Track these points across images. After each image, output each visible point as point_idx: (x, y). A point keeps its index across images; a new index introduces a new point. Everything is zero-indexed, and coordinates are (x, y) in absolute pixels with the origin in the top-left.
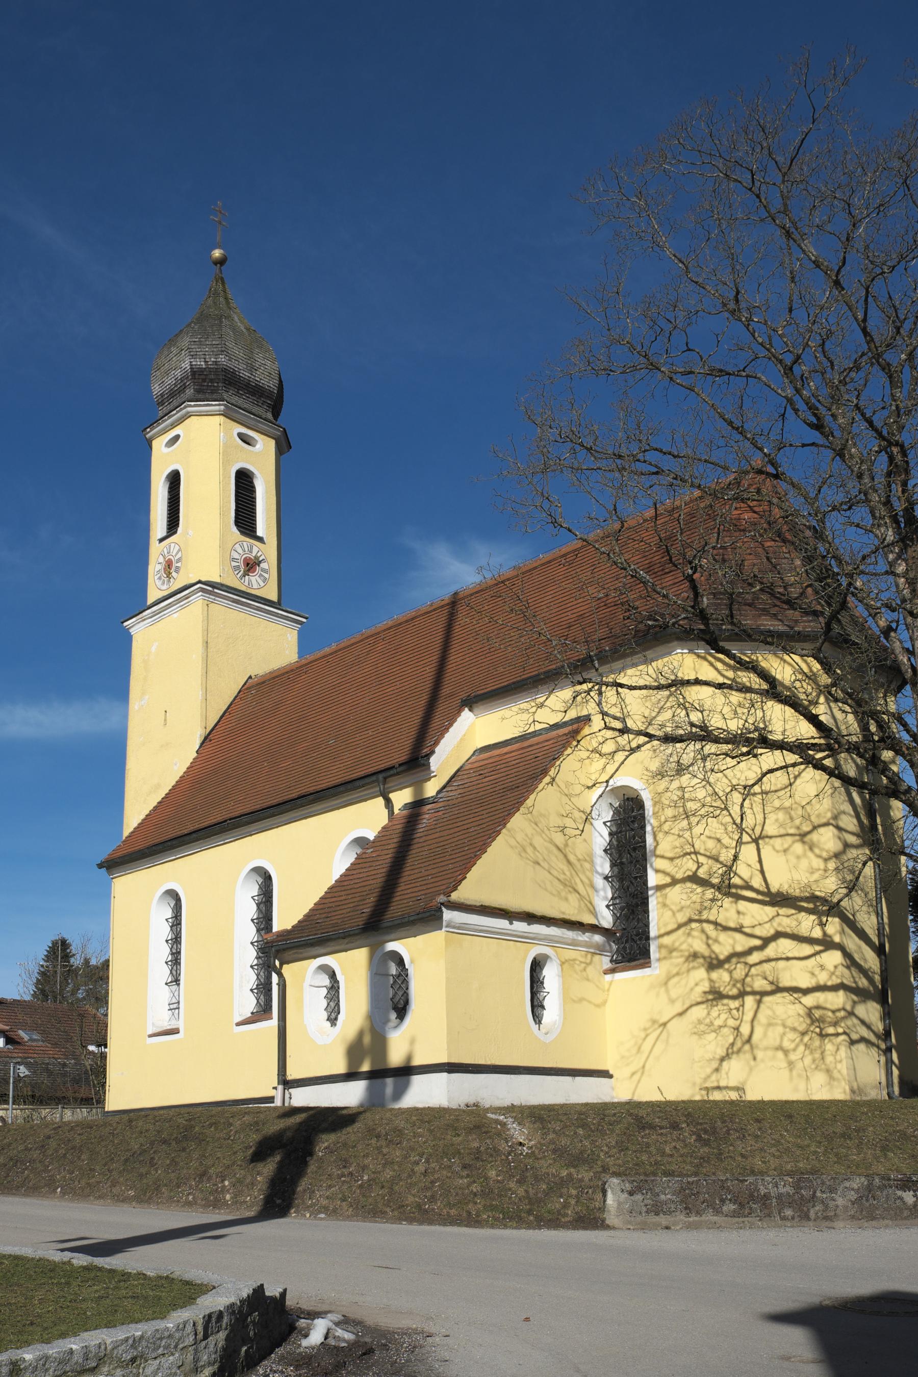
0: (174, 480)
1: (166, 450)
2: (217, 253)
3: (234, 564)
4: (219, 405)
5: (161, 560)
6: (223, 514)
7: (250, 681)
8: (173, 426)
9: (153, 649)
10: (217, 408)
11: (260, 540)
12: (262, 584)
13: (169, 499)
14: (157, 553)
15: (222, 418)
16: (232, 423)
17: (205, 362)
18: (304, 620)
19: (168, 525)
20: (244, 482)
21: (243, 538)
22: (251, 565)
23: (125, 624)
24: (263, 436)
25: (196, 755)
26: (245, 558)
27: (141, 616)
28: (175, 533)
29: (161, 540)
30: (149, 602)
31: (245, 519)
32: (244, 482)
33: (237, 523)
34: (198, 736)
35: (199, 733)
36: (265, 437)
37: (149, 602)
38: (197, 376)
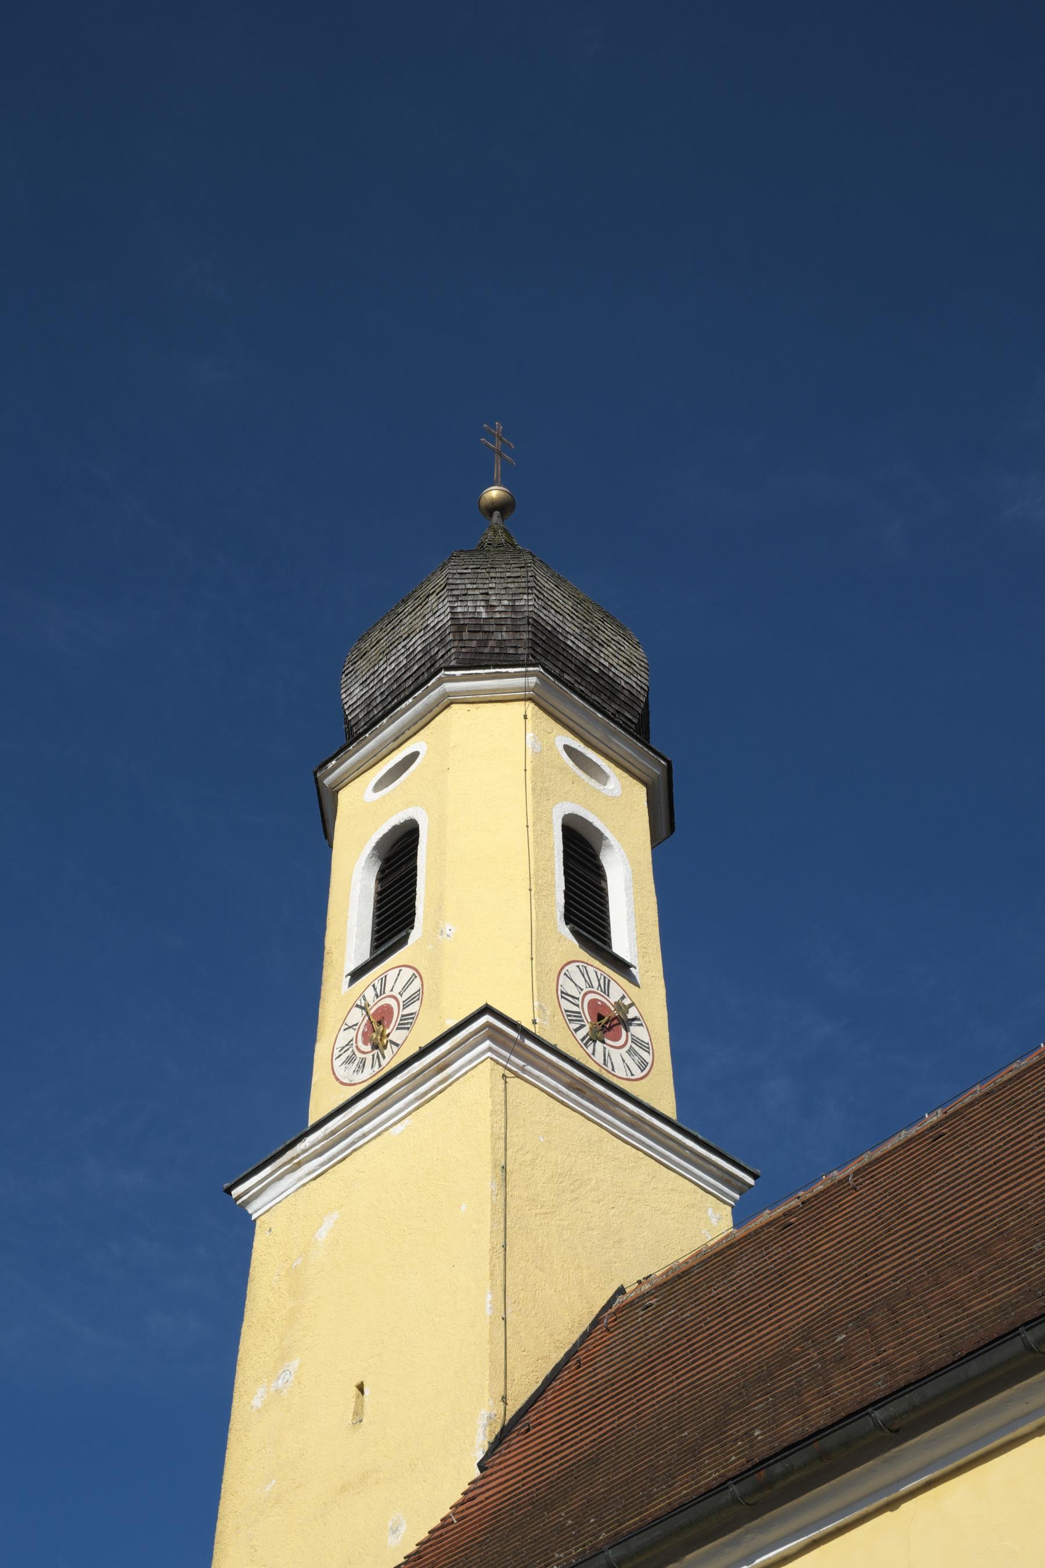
0: (399, 854)
2: (494, 493)
4: (525, 675)
6: (536, 890)
7: (620, 1299)
8: (400, 739)
9: (323, 1234)
10: (520, 681)
12: (638, 1074)
13: (379, 893)
15: (530, 707)
16: (552, 723)
18: (750, 1181)
20: (581, 849)
21: (584, 956)
22: (609, 1023)
23: (235, 1193)
24: (618, 771)
25: (476, 1473)
27: (290, 1154)
31: (586, 909)
32: (581, 849)
33: (569, 917)
34: (482, 1421)
35: (485, 1412)
36: (626, 775)
37: (312, 1121)
38: (466, 635)
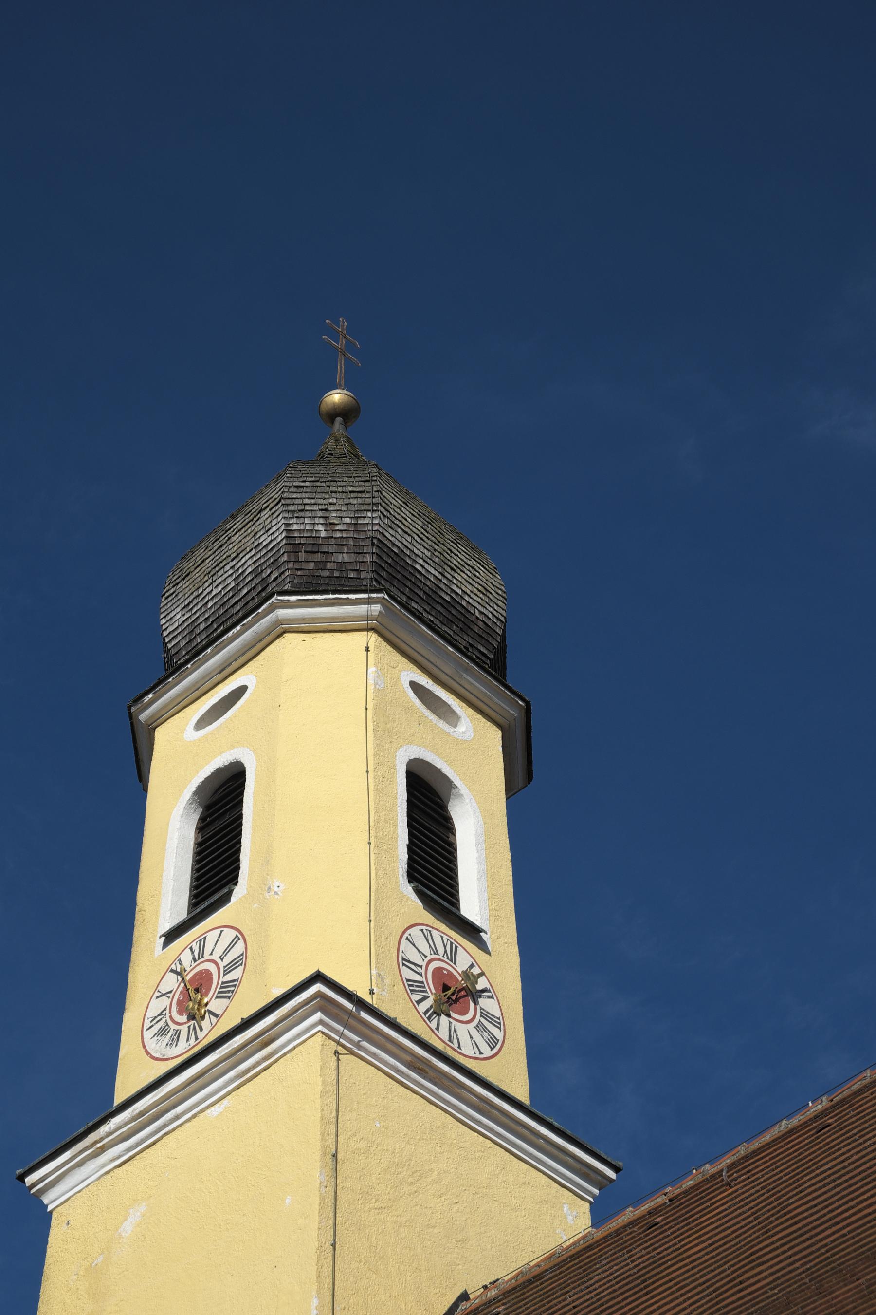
1: (191, 734)
2: (336, 397)
3: (408, 974)
4: (368, 602)
5: (171, 982)
6: (375, 844)
7: (463, 1306)
8: (226, 671)
9: (128, 1228)
10: (362, 609)
11: (471, 931)
12: (487, 1052)
13: (198, 844)
14: (152, 972)
15: (373, 637)
17: (329, 525)
18: (612, 1174)
19: (193, 888)
20: (427, 800)
21: (429, 918)
23: (29, 1180)
24: (471, 711)
26: (438, 971)
28: (225, 900)
29: (171, 936)
30: (119, 1098)
31: (432, 866)
32: (427, 800)
36: (479, 716)
38: (302, 556)
